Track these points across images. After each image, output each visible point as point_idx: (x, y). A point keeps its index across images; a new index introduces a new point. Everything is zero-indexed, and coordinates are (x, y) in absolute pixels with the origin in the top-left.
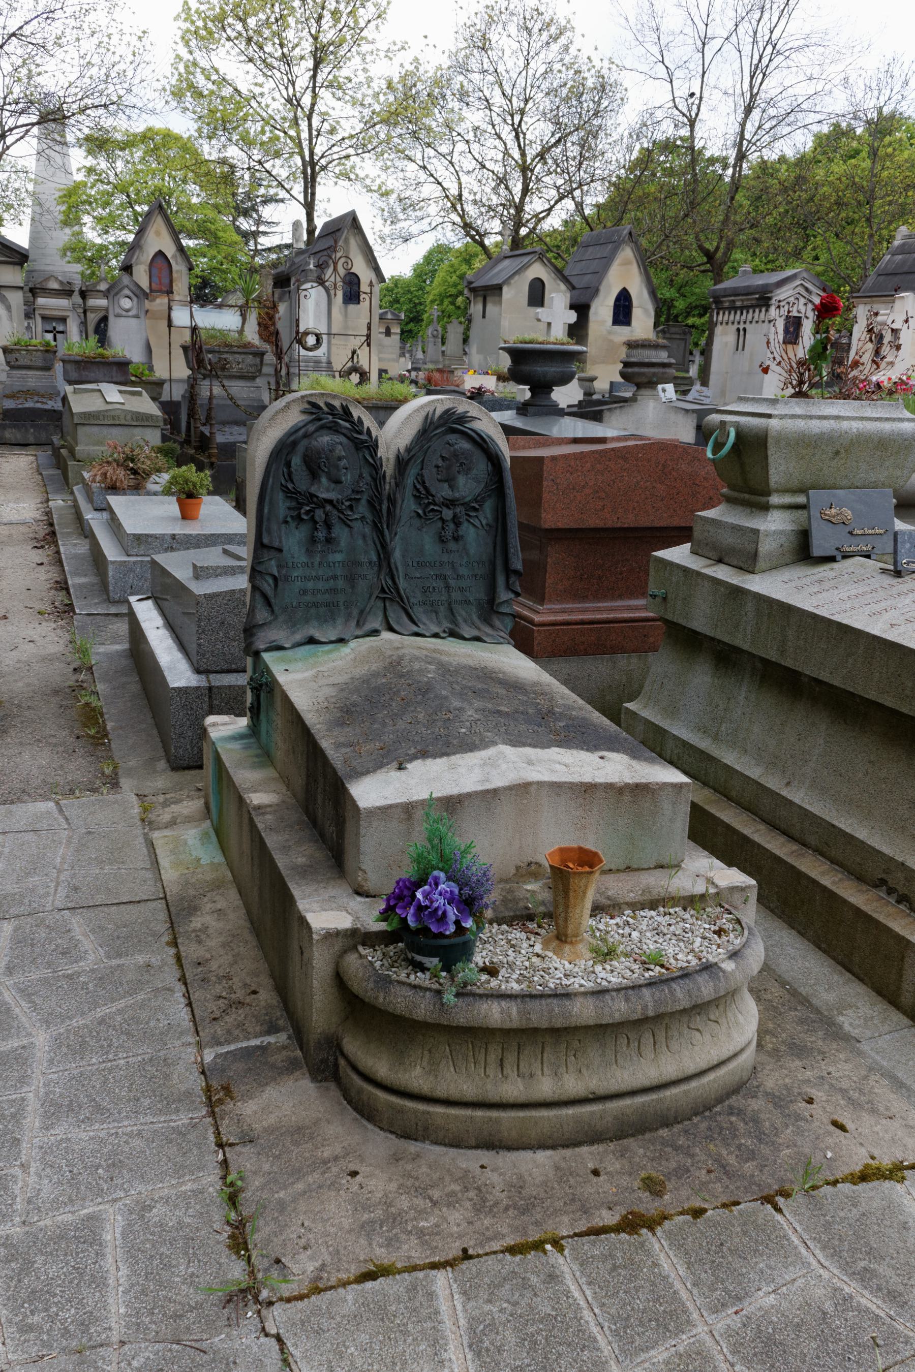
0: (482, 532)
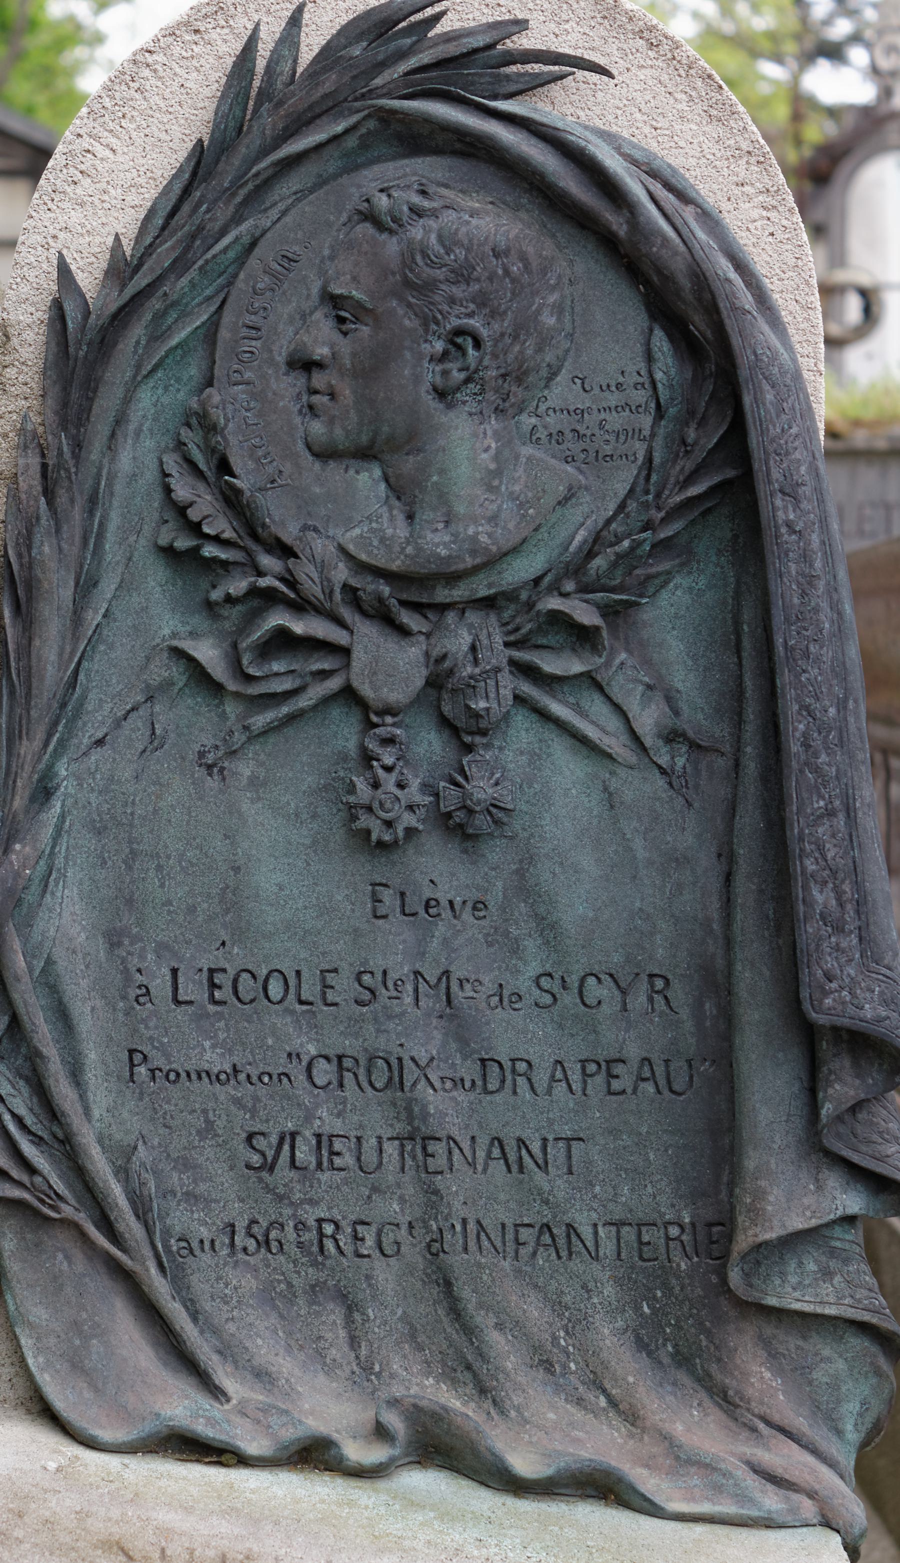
0: (640, 787)
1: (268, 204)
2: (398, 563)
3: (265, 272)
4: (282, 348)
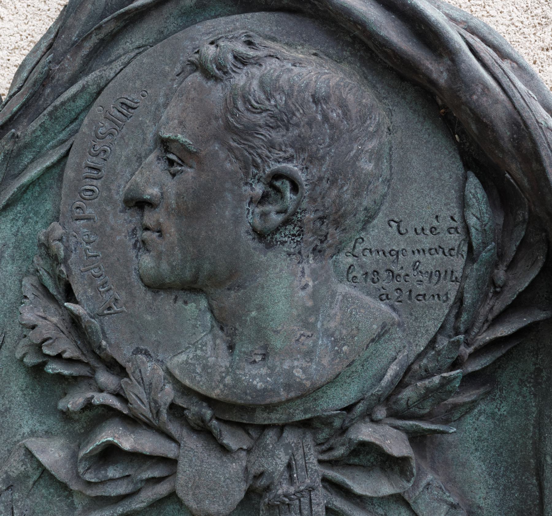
1: (113, 57)
2: (217, 391)
3: (105, 118)
4: (119, 187)
